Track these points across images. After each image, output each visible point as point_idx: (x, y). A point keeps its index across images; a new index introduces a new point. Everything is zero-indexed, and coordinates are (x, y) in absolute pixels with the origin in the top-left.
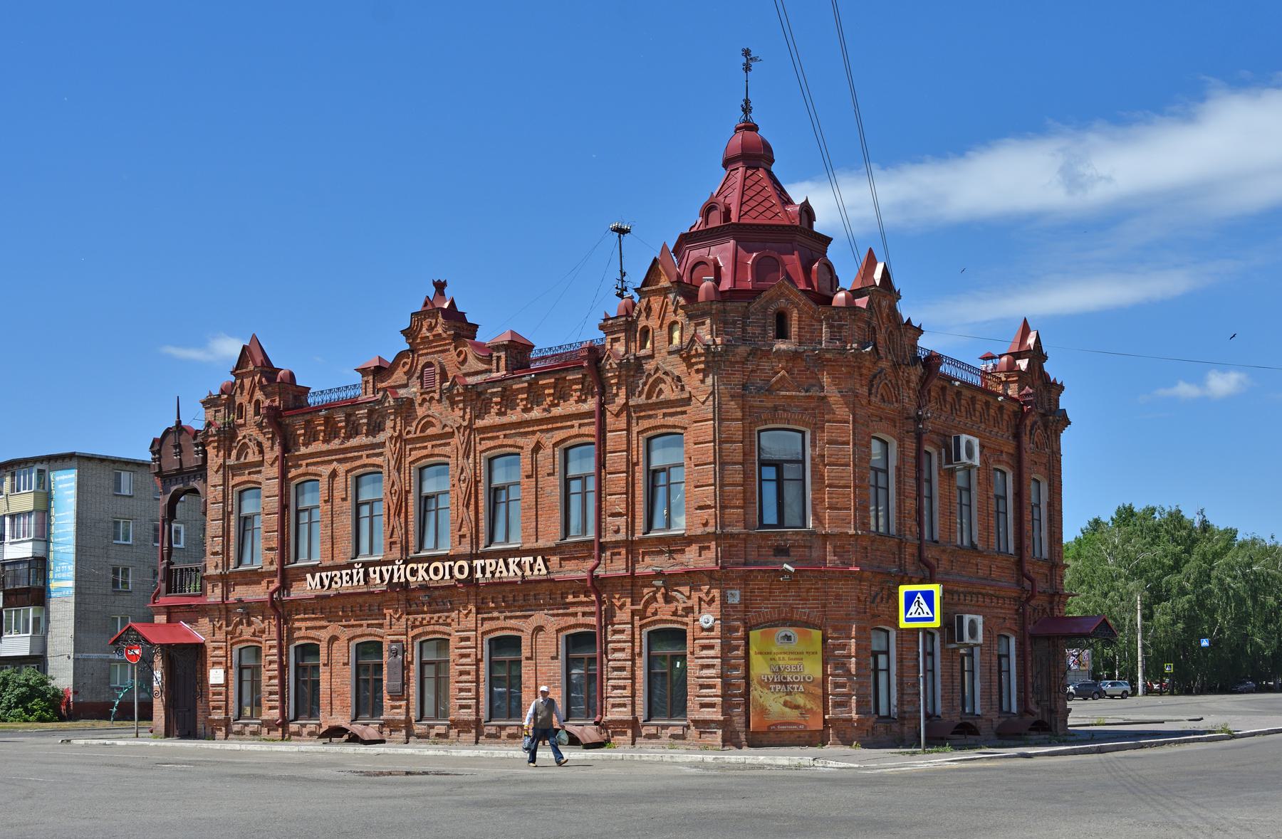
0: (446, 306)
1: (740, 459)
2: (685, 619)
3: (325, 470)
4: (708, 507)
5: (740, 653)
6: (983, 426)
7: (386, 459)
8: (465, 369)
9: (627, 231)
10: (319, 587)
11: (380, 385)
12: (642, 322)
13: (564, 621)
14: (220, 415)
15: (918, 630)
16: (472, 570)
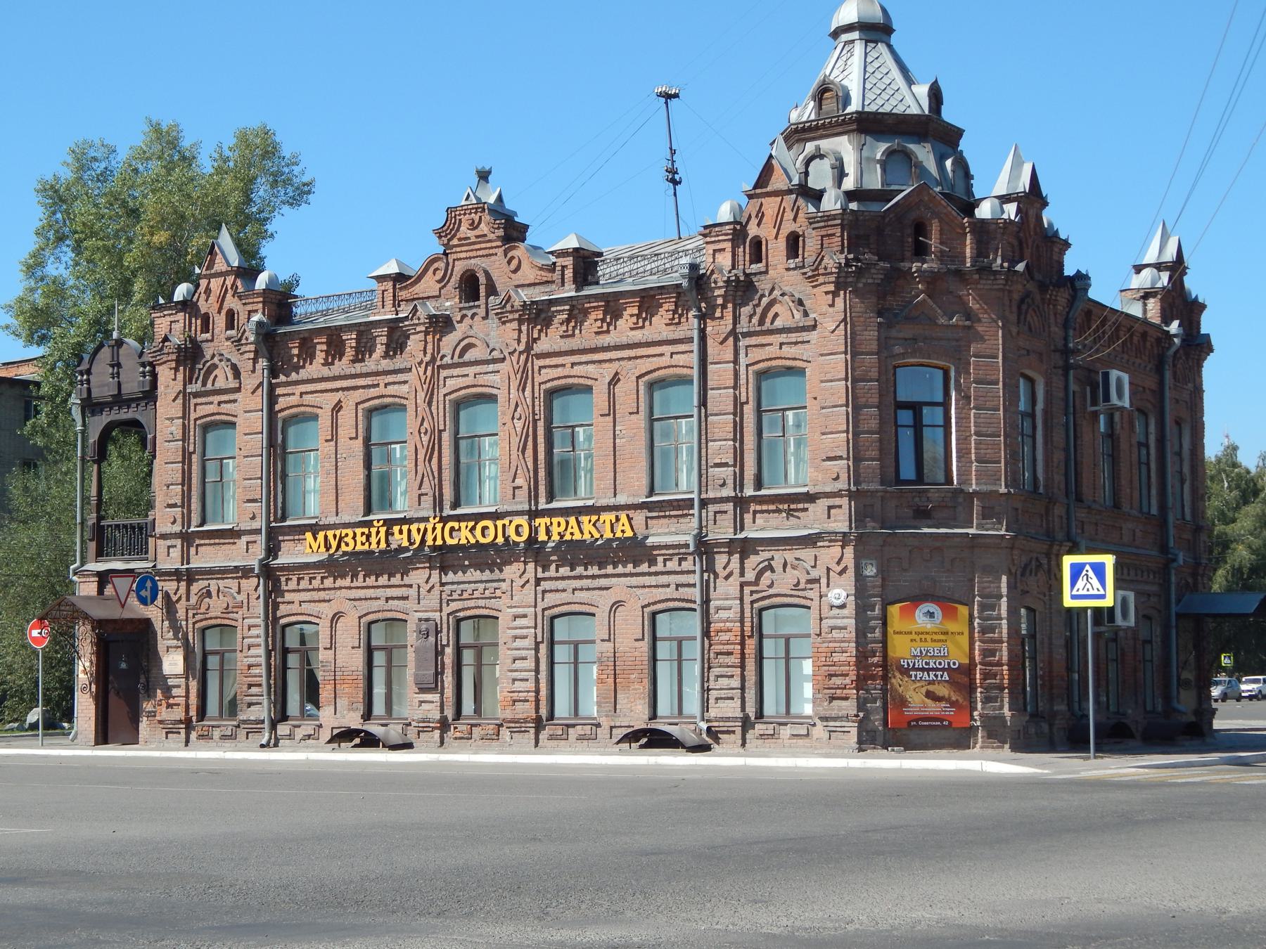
0: (492, 200)
1: (875, 400)
2: (809, 594)
3: (329, 400)
4: (841, 458)
5: (878, 633)
6: (1126, 357)
7: (409, 388)
8: (520, 278)
9: (676, 96)
10: (323, 549)
11: (403, 294)
12: (753, 230)
13: (365, 607)
14: (178, 327)
15: (1085, 609)
16: (534, 531)
